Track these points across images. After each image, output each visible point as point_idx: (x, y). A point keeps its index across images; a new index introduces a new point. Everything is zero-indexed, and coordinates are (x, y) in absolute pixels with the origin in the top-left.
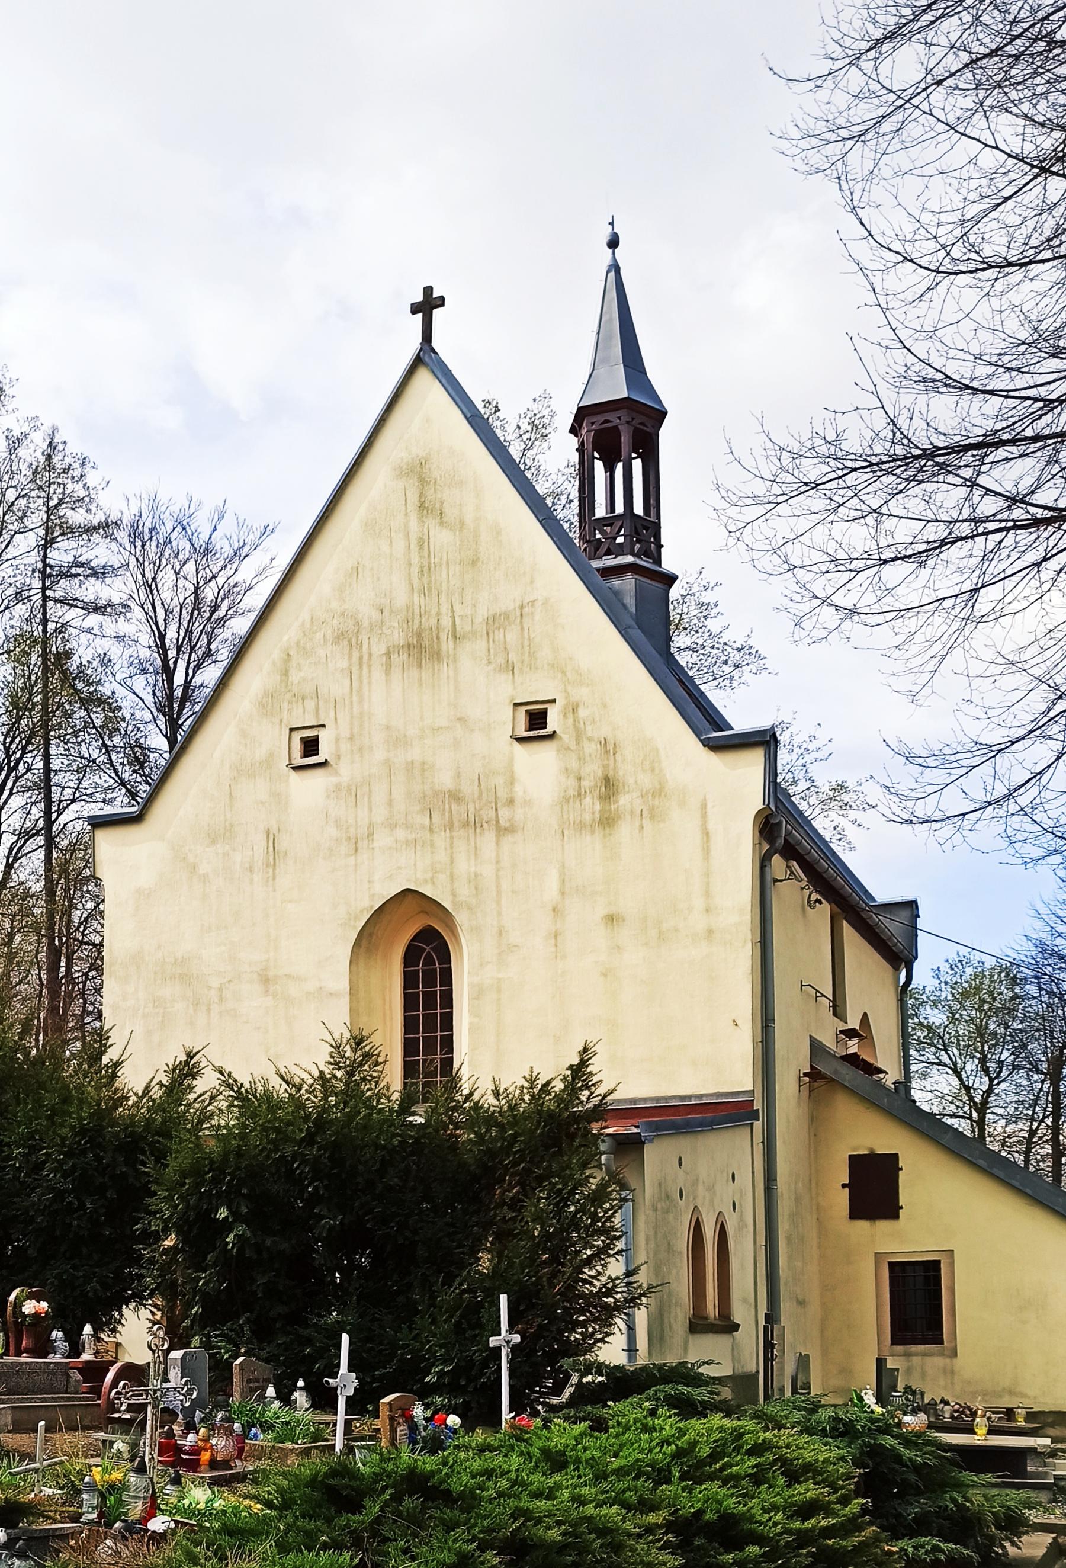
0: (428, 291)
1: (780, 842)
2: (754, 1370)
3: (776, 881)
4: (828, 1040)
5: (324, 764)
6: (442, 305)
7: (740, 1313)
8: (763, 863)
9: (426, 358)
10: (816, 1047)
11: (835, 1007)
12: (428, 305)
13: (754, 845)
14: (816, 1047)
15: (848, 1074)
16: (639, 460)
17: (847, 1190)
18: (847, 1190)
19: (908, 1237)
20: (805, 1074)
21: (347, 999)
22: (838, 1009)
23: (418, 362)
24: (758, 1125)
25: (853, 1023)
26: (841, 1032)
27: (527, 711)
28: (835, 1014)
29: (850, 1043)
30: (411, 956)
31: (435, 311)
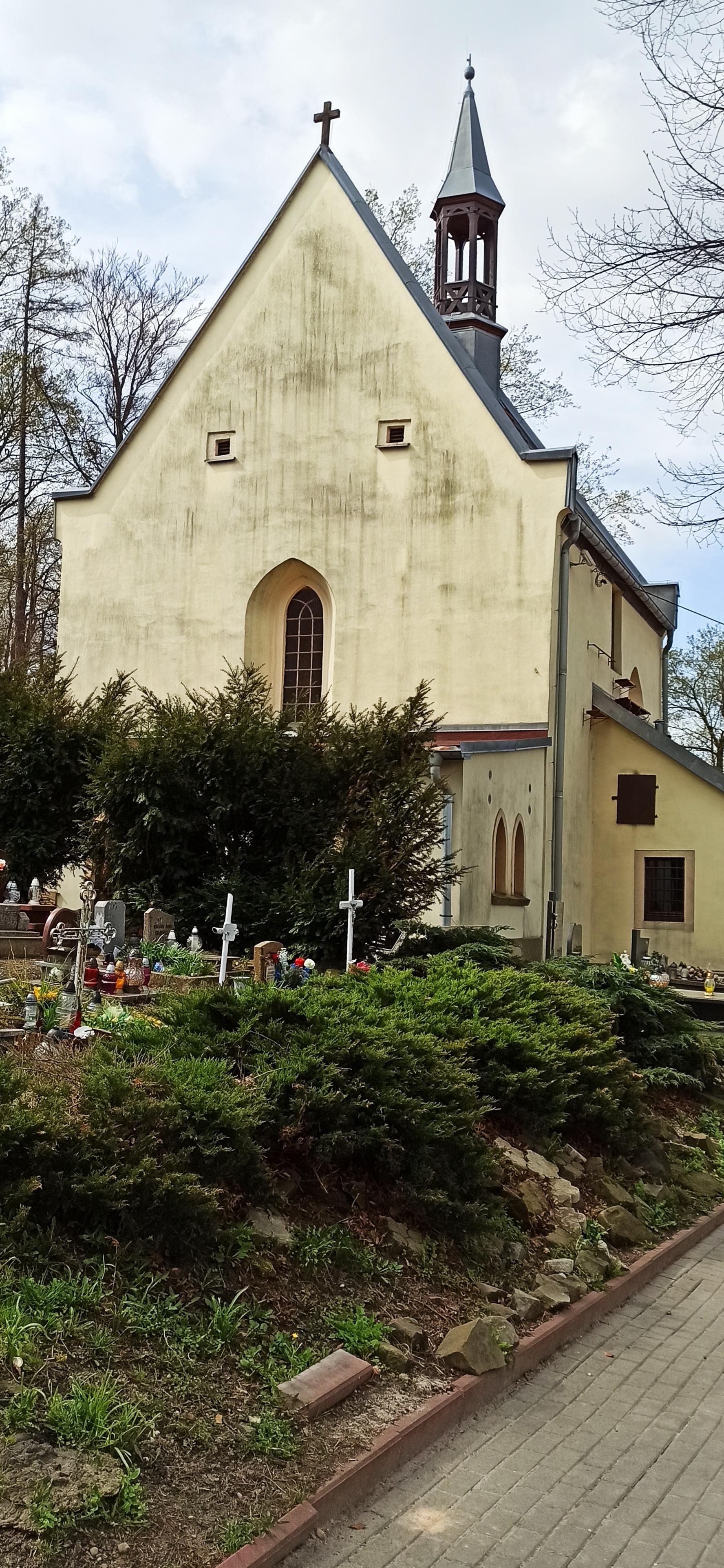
0: (328, 105)
1: (576, 535)
2: (539, 935)
3: (572, 564)
4: (606, 686)
5: (233, 461)
6: (338, 116)
7: (530, 892)
8: (563, 550)
9: (323, 156)
10: (597, 692)
11: (612, 662)
12: (327, 116)
13: (557, 536)
14: (597, 692)
15: (620, 714)
16: (482, 241)
17: (616, 801)
18: (616, 801)
19: (660, 839)
20: (588, 712)
21: (243, 640)
22: (614, 663)
23: (317, 159)
24: (550, 749)
25: (626, 675)
26: (617, 681)
27: (389, 427)
28: (612, 667)
29: (623, 690)
30: (292, 610)
31: (332, 121)
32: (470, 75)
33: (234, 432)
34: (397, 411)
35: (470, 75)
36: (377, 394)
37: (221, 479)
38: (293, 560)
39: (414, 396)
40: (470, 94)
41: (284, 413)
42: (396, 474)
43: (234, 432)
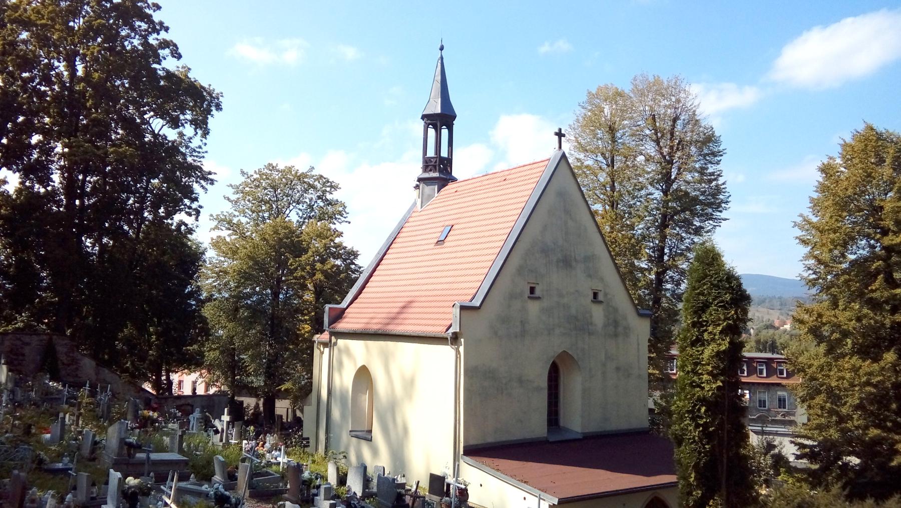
32: (442, 49)
34: (598, 286)
35: (442, 49)
36: (590, 276)
37: (534, 307)
39: (602, 279)
40: (442, 58)
41: (556, 279)
42: (598, 313)
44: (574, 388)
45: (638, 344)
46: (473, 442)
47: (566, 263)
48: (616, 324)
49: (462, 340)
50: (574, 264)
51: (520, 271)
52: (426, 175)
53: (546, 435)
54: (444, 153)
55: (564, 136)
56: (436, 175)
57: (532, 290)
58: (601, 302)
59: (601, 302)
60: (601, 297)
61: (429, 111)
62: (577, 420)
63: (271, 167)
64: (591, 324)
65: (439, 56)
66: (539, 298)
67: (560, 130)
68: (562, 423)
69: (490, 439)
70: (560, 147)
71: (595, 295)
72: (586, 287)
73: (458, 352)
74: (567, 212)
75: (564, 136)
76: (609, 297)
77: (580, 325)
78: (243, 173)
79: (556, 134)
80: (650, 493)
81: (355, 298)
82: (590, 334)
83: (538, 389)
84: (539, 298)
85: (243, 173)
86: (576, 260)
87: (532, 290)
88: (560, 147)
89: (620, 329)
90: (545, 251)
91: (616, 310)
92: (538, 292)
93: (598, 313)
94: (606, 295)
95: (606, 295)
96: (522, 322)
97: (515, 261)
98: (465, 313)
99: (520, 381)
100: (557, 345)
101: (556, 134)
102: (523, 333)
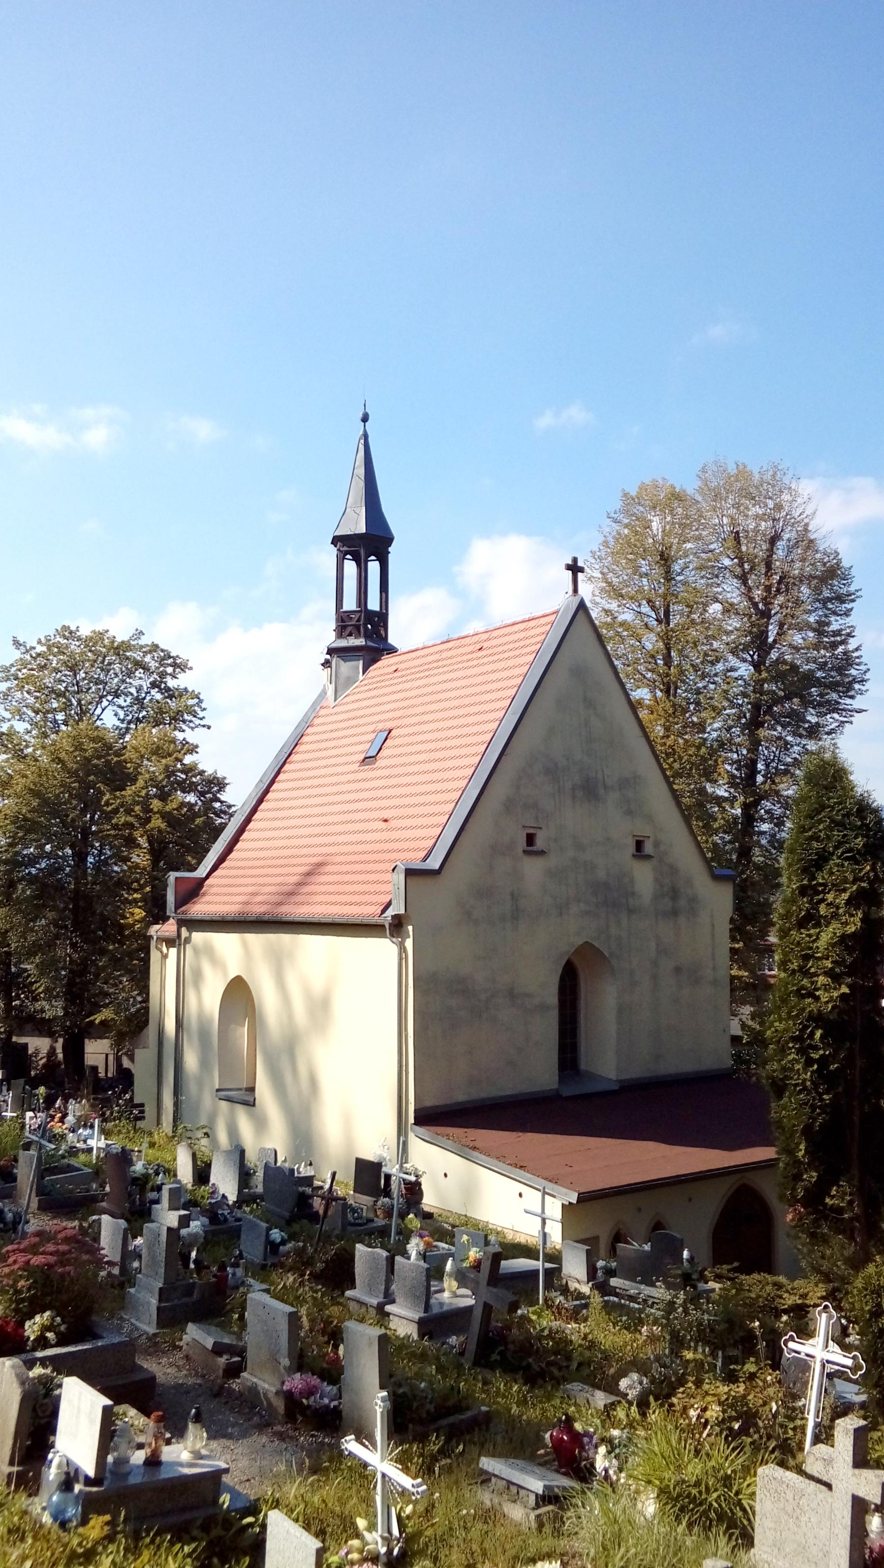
32: (365, 419)
33: (541, 828)
34: (643, 829)
35: (365, 419)
36: (629, 813)
37: (533, 868)
38: (587, 942)
40: (366, 436)
41: (572, 819)
42: (644, 877)
43: (541, 828)
44: (605, 1006)
45: (713, 925)
46: (429, 1102)
47: (590, 790)
48: (675, 894)
49: (410, 928)
50: (602, 791)
51: (509, 806)
52: (343, 643)
53: (555, 1086)
54: (374, 604)
55: (582, 570)
56: (360, 642)
57: (530, 839)
58: (649, 857)
59: (649, 857)
60: (648, 848)
61: (343, 531)
62: (608, 1060)
63: (68, 633)
64: (633, 894)
65: (361, 432)
66: (542, 853)
67: (575, 560)
68: (583, 1066)
69: (461, 1096)
70: (575, 590)
71: (639, 845)
72: (623, 831)
73: (402, 949)
74: (589, 703)
75: (582, 570)
76: (662, 848)
77: (612, 897)
78: (17, 643)
79: (568, 567)
80: (738, 1176)
81: (221, 860)
82: (631, 911)
83: (543, 1008)
84: (542, 853)
85: (17, 643)
86: (606, 787)
87: (530, 839)
88: (575, 590)
89: (683, 903)
90: (553, 772)
91: (674, 870)
92: (540, 843)
93: (644, 877)
94: (657, 844)
95: (657, 844)
96: (512, 894)
97: (500, 790)
98: (413, 881)
99: (512, 995)
100: (571, 932)
101: (568, 567)
102: (516, 915)
